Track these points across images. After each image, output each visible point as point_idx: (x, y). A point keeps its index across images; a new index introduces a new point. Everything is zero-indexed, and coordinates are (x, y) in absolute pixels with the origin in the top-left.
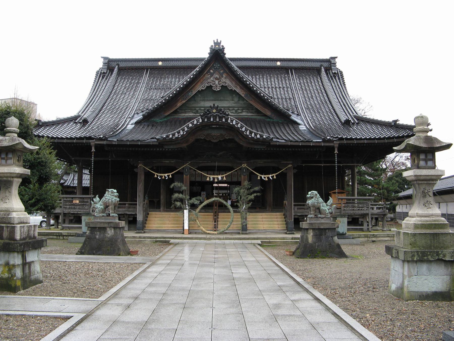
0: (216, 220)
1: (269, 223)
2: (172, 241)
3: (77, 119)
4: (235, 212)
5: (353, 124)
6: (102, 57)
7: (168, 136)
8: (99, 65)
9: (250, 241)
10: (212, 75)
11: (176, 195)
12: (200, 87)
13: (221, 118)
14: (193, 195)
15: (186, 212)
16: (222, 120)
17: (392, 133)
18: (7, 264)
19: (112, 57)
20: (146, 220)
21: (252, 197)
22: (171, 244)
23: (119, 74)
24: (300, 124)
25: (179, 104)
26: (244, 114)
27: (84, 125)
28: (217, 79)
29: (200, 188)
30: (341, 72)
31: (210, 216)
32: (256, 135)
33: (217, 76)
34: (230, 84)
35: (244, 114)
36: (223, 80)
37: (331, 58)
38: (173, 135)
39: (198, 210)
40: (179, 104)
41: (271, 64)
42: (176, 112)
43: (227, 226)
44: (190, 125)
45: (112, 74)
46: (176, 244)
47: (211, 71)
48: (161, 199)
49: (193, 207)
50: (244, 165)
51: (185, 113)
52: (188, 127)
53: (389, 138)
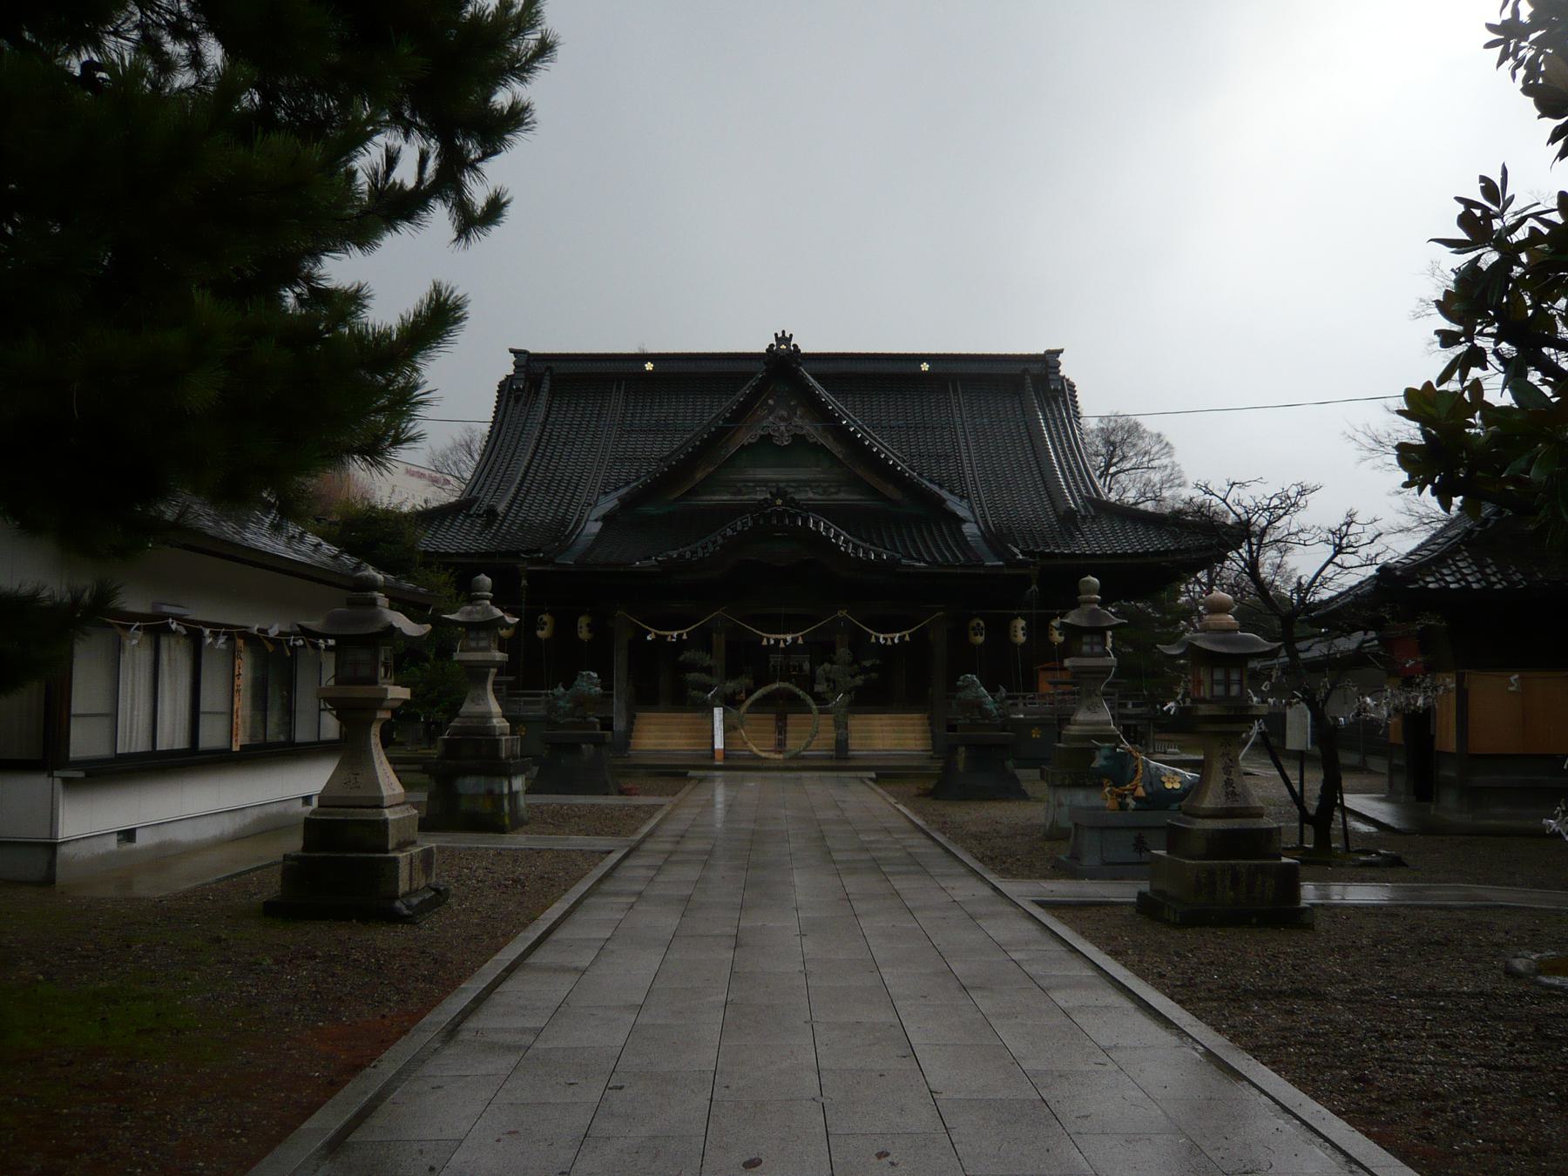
0: (782, 730)
1: (893, 735)
2: (691, 773)
3: (470, 508)
4: (821, 712)
5: (1084, 518)
6: (511, 351)
7: (681, 556)
8: (506, 367)
9: (853, 774)
10: (771, 410)
11: (692, 676)
12: (747, 437)
13: (793, 518)
14: (732, 672)
15: (718, 713)
16: (795, 522)
17: (1154, 542)
18: (490, 793)
19: (534, 349)
20: (631, 730)
21: (859, 680)
22: (691, 778)
23: (553, 393)
24: (964, 521)
25: (699, 476)
26: (842, 496)
27: (489, 524)
28: (782, 419)
29: (748, 662)
30: (1072, 386)
31: (768, 721)
32: (866, 553)
33: (784, 413)
34: (812, 431)
35: (842, 496)
36: (797, 421)
37: (1048, 352)
38: (693, 553)
39: (743, 709)
40: (699, 476)
41: (907, 368)
42: (692, 492)
43: (804, 743)
44: (729, 532)
45: (537, 393)
46: (701, 780)
47: (771, 402)
48: (665, 684)
49: (730, 702)
50: (842, 613)
51: (713, 493)
52: (724, 537)
53: (1157, 553)
